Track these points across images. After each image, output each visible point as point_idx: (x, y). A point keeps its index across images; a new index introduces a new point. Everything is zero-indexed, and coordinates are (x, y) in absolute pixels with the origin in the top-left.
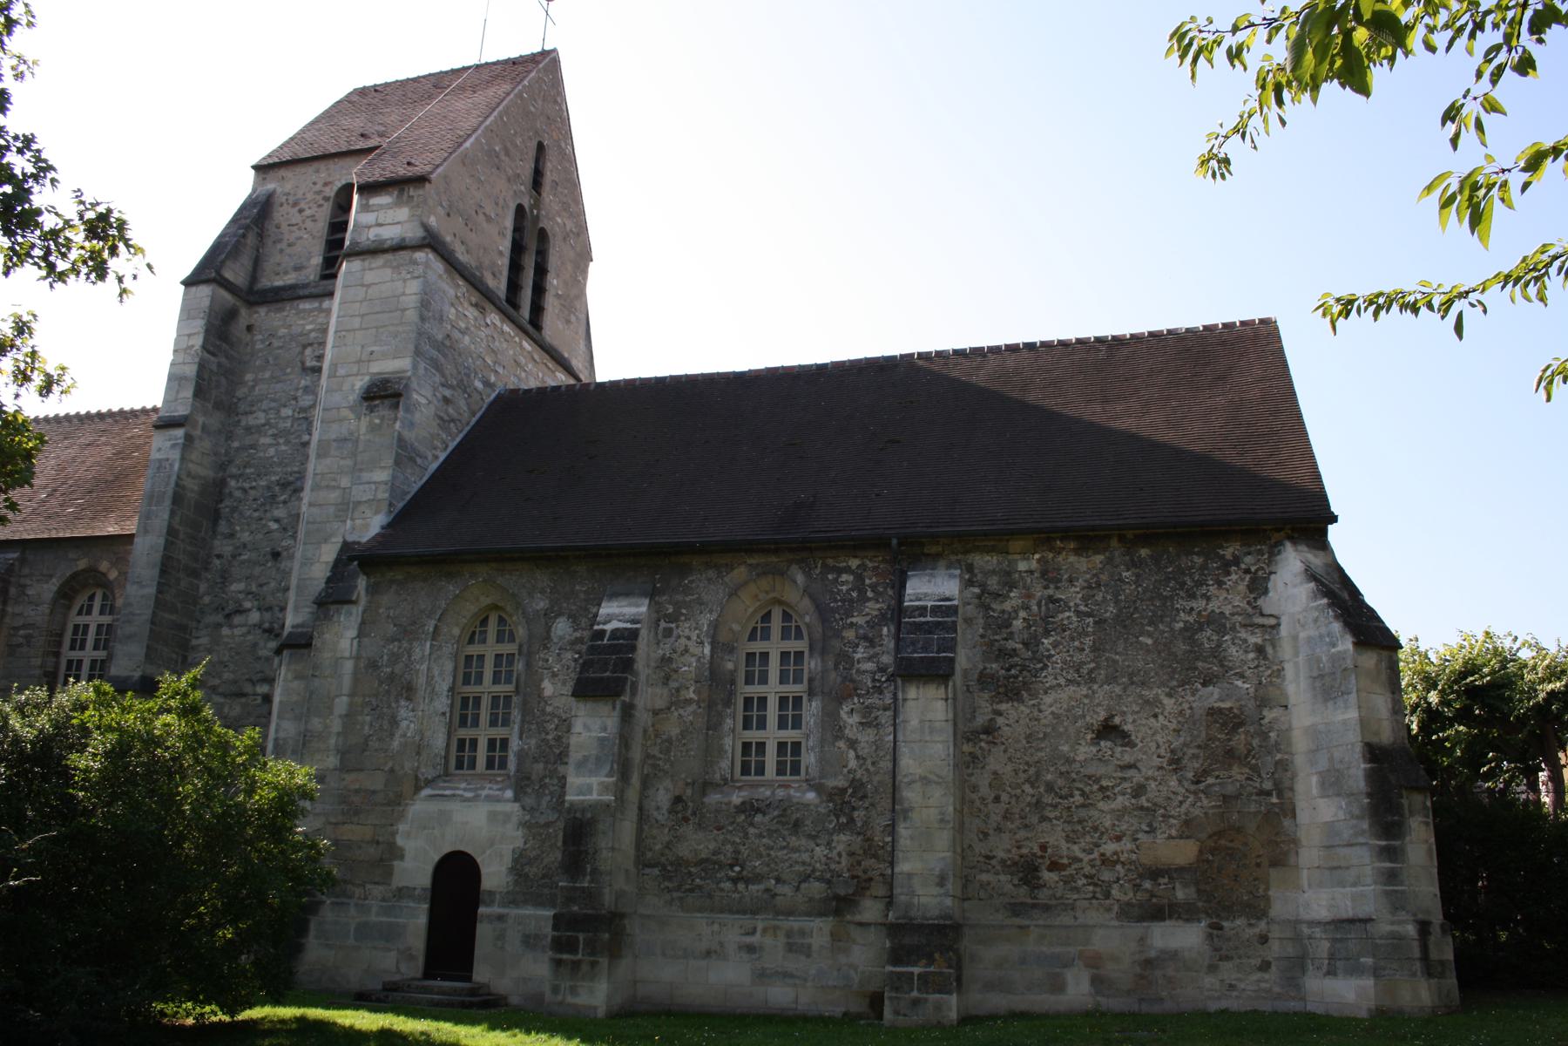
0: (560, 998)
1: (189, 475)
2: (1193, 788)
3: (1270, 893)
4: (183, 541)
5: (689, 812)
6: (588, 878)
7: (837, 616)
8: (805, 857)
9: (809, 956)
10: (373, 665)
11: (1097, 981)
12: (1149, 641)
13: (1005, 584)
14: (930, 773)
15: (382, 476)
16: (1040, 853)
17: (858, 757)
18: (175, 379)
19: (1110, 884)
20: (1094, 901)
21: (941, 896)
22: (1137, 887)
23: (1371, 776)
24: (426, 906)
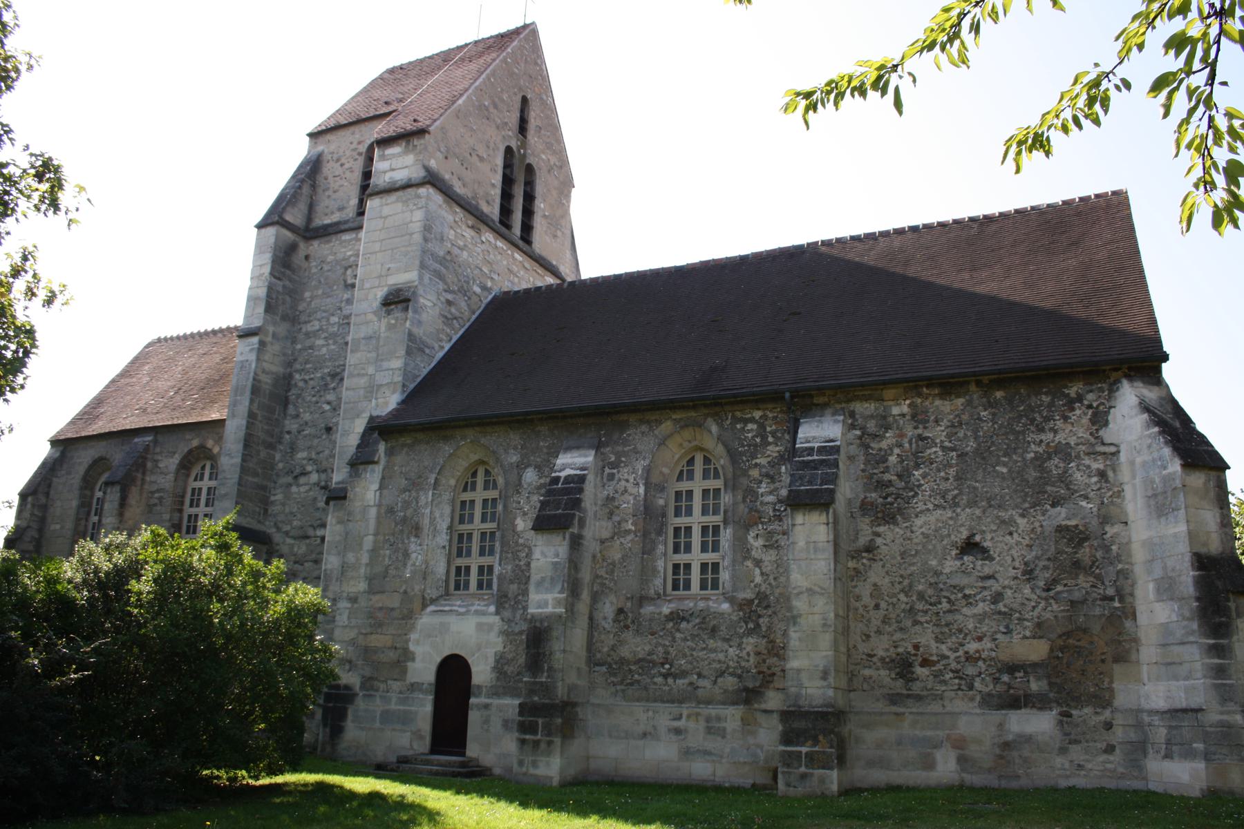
0: (524, 769)
1: (264, 371)
2: (1044, 594)
3: (1114, 685)
4: (261, 422)
5: (629, 621)
6: (545, 674)
7: (744, 458)
8: (721, 656)
9: (724, 737)
10: (391, 511)
11: (962, 760)
12: (1005, 470)
13: (882, 426)
14: (815, 585)
15: (397, 363)
16: (913, 652)
17: (762, 574)
18: (252, 299)
19: (973, 678)
20: (960, 692)
21: (823, 687)
22: (996, 680)
23: (1200, 583)
24: (431, 697)
